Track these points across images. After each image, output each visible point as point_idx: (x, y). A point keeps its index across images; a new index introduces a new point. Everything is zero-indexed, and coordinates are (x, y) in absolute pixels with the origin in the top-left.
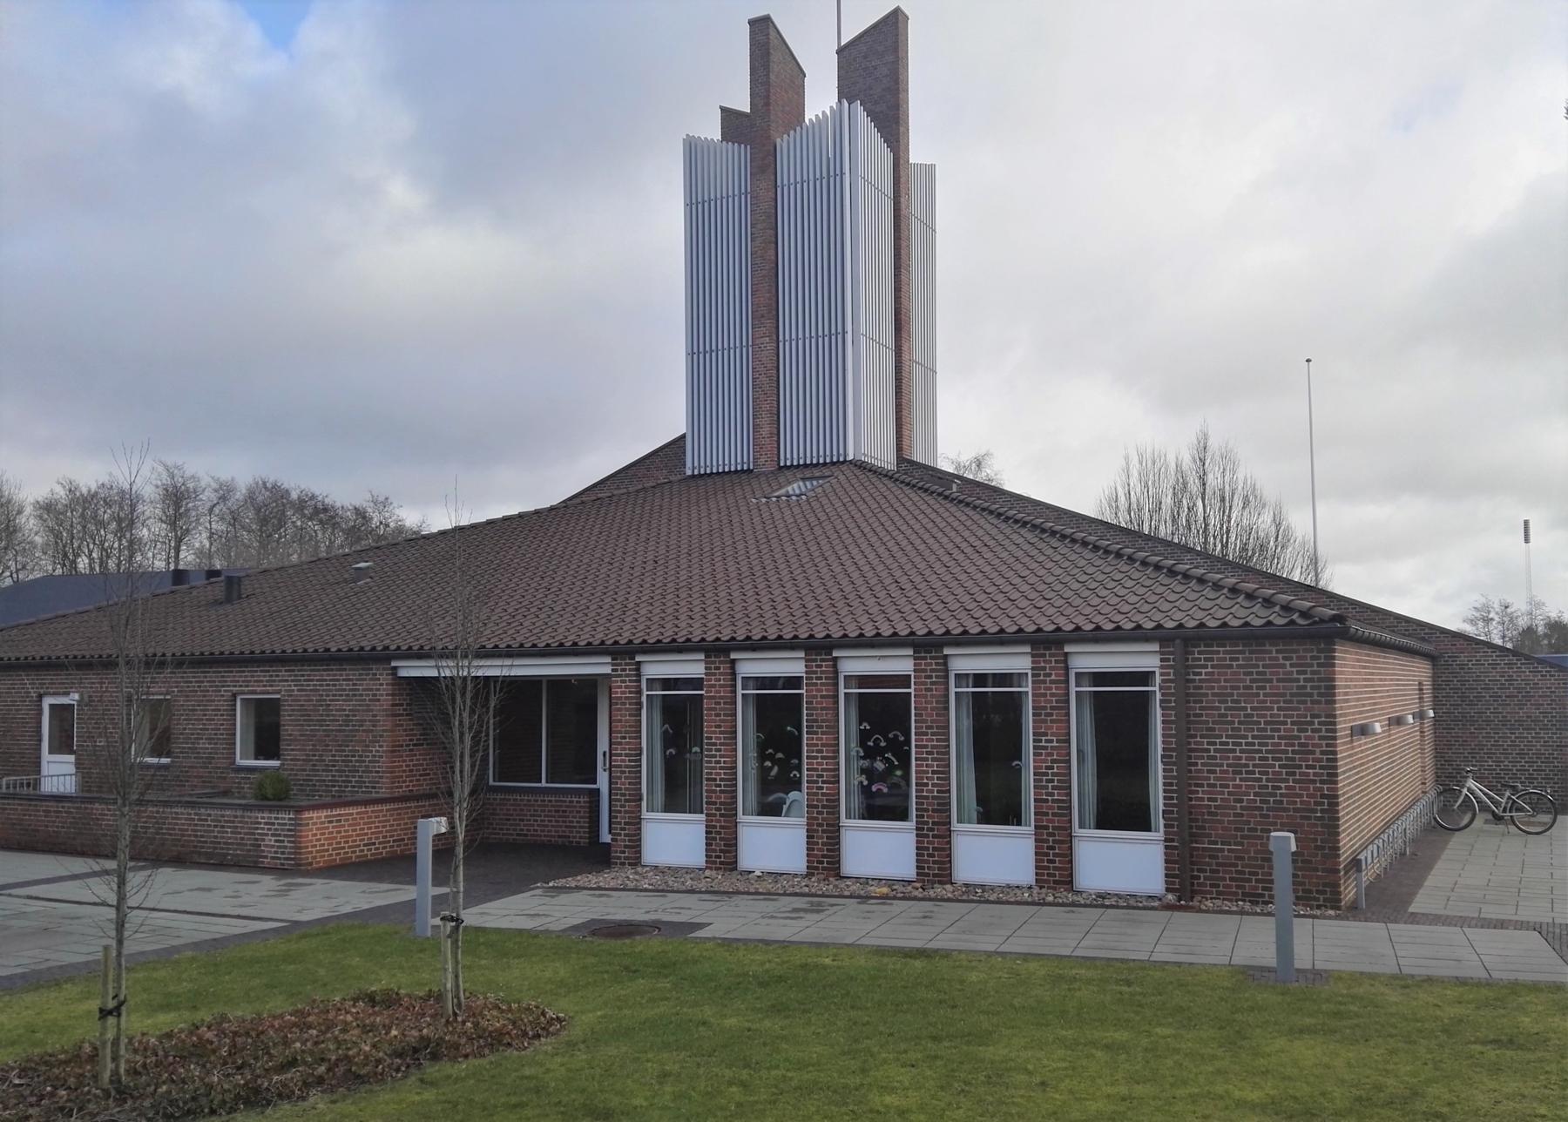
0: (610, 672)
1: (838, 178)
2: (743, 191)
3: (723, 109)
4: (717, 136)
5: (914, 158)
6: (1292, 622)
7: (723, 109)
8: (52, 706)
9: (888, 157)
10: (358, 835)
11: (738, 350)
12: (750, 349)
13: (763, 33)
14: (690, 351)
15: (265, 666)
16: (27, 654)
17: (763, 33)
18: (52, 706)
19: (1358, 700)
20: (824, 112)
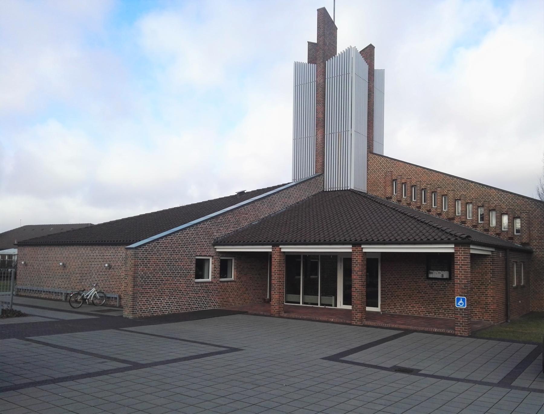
0: (271, 251)
1: (348, 75)
2: (307, 136)
3: (308, 42)
4: (306, 61)
5: (376, 67)
6: (456, 239)
7: (308, 42)
8: (516, 233)
9: (366, 67)
10: (195, 300)
11: (313, 137)
12: (315, 137)
13: (323, 16)
14: (293, 179)
15: (465, 246)
16: (78, 240)
17: (323, 16)
18: (516, 233)
19: (497, 264)
20: (344, 51)
